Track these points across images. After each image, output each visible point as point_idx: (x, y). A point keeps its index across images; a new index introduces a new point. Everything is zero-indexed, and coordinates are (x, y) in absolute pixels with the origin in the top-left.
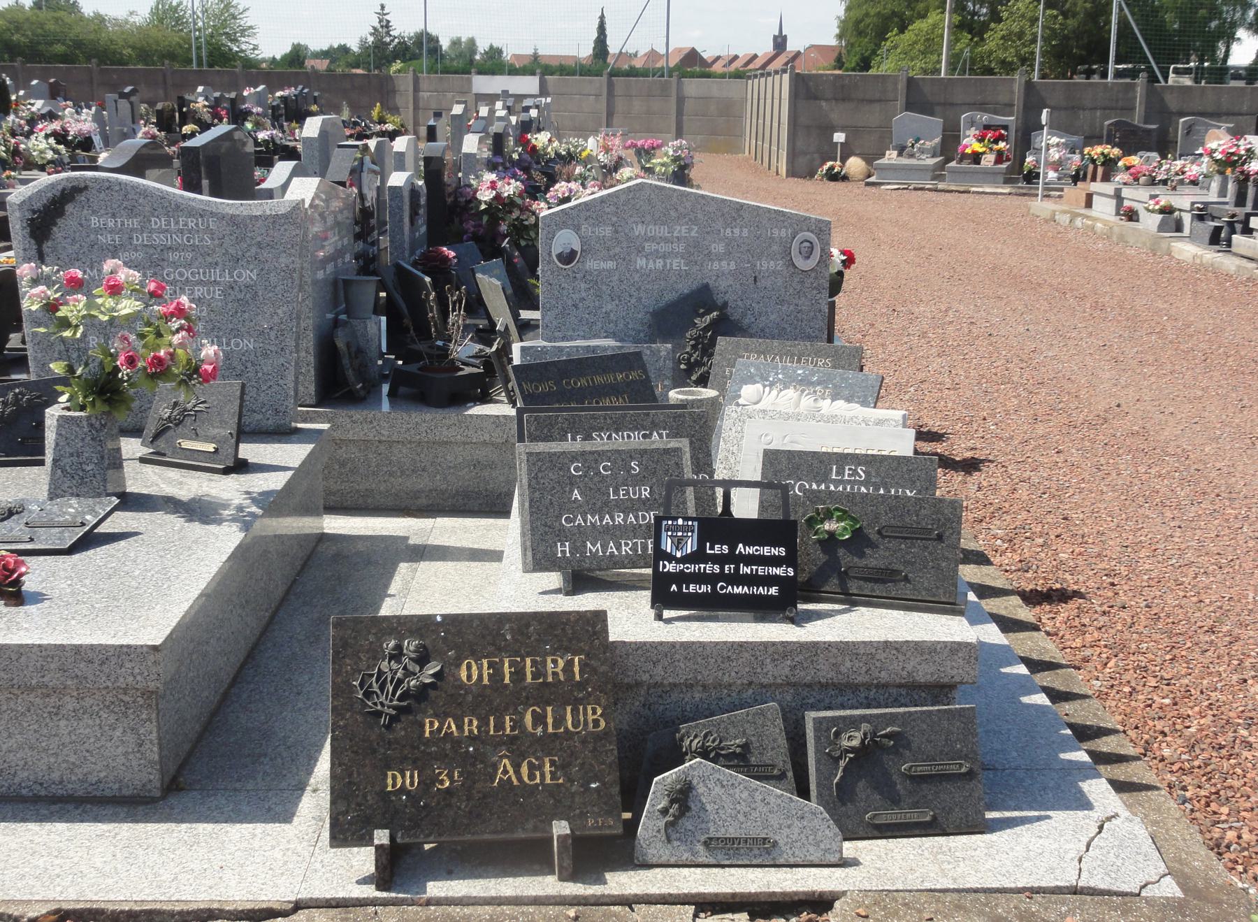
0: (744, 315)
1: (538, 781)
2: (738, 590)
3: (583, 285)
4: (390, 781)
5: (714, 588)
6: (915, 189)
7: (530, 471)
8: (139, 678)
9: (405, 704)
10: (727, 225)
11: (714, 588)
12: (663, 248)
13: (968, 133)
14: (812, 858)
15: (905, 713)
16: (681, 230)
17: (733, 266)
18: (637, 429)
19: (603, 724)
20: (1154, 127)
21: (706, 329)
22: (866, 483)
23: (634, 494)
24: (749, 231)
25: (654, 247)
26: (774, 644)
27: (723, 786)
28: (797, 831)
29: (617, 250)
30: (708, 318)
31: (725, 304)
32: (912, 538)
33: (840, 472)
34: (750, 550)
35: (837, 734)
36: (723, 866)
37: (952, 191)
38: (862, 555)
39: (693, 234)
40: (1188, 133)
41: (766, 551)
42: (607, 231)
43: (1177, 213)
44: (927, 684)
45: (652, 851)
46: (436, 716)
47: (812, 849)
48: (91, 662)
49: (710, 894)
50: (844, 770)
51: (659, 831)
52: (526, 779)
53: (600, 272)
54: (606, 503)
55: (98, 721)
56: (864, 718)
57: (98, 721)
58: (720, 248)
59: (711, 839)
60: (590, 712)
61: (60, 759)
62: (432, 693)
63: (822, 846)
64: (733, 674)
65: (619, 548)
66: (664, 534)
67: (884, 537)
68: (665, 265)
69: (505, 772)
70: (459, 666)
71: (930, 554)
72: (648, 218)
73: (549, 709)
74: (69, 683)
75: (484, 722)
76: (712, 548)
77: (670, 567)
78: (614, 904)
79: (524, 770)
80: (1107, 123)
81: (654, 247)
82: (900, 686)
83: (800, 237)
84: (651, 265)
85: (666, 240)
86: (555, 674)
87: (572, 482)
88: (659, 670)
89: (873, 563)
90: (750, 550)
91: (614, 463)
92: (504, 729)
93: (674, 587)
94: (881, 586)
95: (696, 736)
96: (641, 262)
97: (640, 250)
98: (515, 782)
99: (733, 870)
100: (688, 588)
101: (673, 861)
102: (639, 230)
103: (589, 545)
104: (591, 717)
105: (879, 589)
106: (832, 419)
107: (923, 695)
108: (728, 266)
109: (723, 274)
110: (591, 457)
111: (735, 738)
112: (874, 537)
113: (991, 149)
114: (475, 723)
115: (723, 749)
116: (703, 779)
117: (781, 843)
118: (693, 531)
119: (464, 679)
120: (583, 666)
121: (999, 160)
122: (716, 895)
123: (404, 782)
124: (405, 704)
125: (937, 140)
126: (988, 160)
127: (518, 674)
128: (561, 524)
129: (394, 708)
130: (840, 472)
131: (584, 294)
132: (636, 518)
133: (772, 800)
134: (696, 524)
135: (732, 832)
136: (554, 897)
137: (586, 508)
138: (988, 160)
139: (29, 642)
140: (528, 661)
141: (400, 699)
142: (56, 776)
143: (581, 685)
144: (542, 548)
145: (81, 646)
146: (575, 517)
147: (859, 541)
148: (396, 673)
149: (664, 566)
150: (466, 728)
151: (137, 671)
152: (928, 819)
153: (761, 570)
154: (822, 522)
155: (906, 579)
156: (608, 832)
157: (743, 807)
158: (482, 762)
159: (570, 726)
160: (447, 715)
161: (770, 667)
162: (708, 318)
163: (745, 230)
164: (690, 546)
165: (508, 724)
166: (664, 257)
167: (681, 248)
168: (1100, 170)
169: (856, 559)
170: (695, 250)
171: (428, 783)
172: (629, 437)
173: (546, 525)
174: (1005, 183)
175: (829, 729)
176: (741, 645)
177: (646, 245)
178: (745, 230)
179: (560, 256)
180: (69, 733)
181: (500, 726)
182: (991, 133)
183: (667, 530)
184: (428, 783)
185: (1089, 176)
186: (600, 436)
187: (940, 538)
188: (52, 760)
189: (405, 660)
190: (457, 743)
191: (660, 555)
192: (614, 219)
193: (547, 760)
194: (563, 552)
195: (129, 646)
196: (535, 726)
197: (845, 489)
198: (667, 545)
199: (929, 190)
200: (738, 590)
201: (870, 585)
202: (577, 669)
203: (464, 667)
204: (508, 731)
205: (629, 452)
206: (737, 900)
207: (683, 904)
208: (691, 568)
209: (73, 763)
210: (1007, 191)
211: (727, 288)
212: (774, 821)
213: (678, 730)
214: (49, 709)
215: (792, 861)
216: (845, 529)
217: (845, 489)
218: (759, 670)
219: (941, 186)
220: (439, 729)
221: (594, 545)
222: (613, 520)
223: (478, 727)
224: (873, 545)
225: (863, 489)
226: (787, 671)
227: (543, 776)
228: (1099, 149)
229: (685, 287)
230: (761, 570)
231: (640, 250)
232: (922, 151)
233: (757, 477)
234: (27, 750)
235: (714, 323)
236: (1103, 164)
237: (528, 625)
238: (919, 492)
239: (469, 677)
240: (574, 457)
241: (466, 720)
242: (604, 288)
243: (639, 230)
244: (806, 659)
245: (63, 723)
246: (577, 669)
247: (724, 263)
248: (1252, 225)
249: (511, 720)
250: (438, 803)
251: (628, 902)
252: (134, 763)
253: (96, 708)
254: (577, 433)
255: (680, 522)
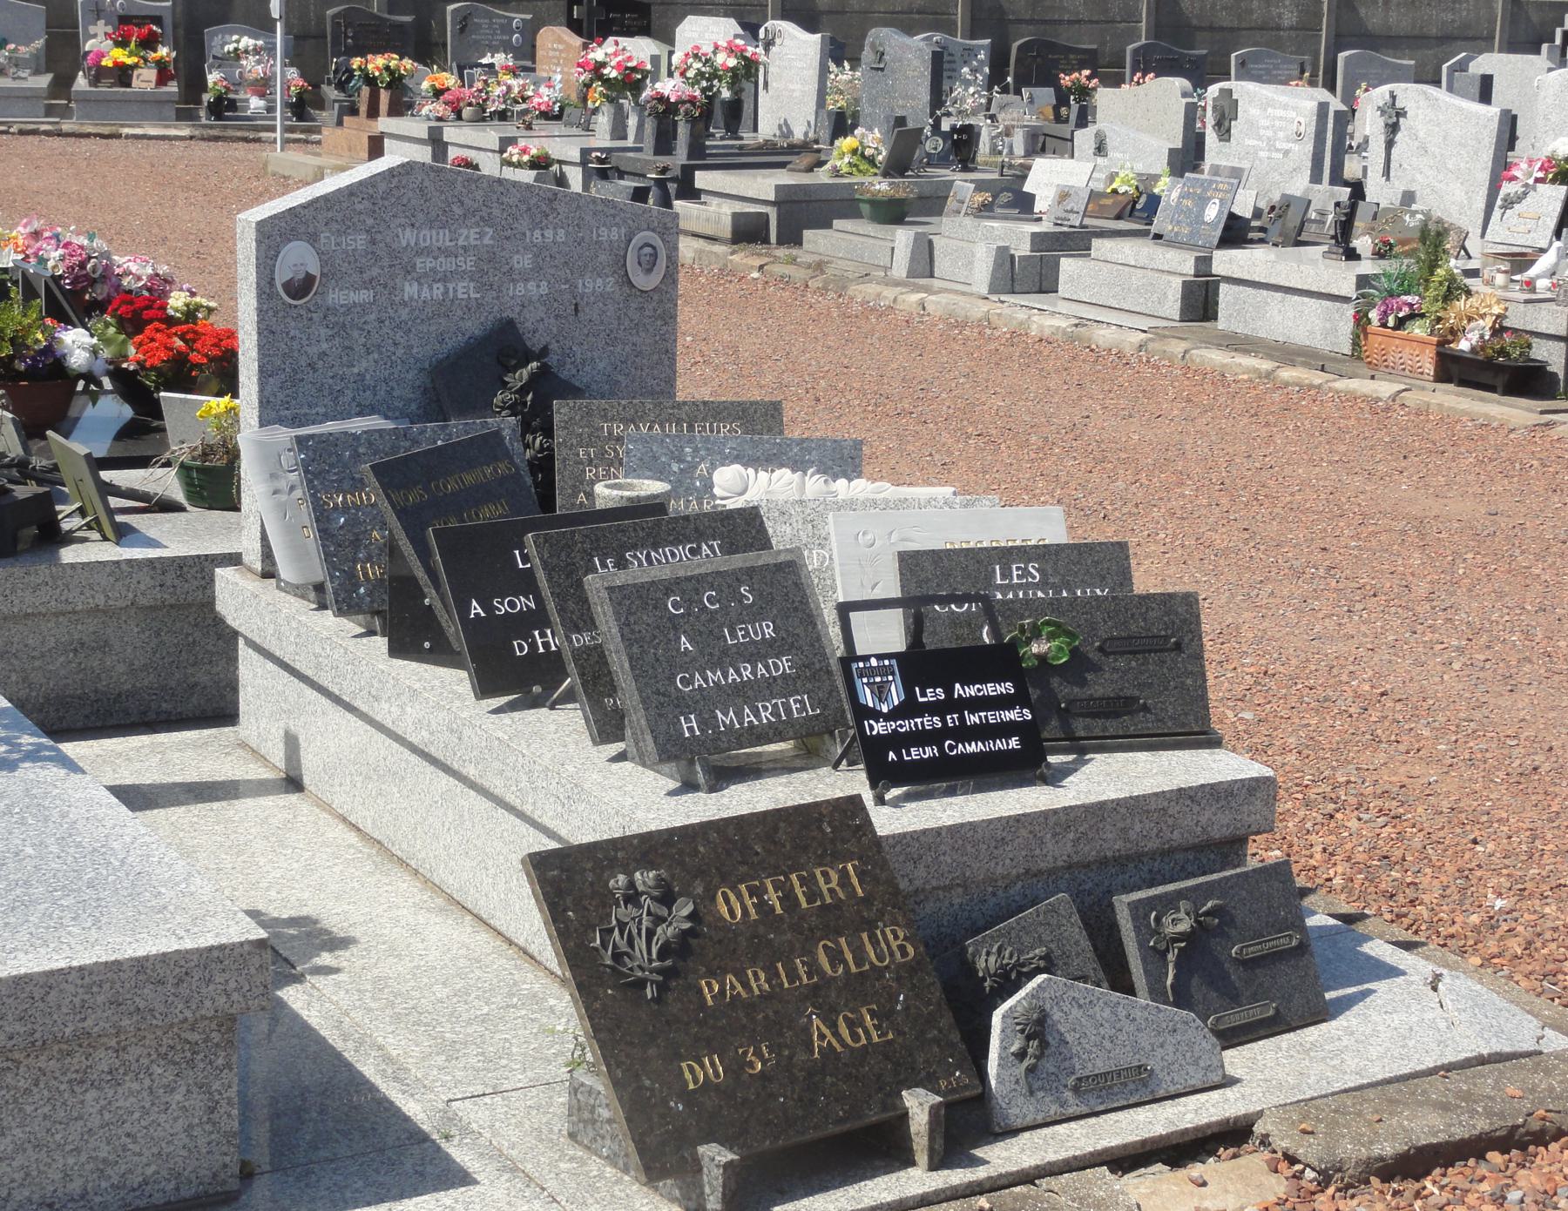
0: (562, 364)
1: (864, 1041)
2: (973, 748)
3: (323, 331)
4: (688, 1076)
5: (941, 749)
6: (22, 133)
7: (617, 614)
8: (235, 996)
9: (669, 963)
10: (535, 225)
11: (941, 749)
12: (445, 264)
13: (92, 30)
14: (1193, 1082)
15: (1221, 880)
16: (467, 235)
17: (544, 290)
18: (681, 542)
19: (910, 950)
20: (408, 19)
21: (523, 391)
22: (1043, 585)
23: (756, 633)
24: (567, 234)
25: (430, 263)
26: (1055, 811)
27: (1080, 1006)
28: (1171, 1049)
29: (375, 271)
30: (525, 373)
31: (545, 351)
32: (1144, 652)
33: (1006, 574)
34: (971, 691)
35: (1158, 919)
36: (1097, 1114)
37: (88, 135)
38: (1083, 683)
39: (487, 241)
40: (462, 30)
41: (990, 689)
42: (359, 241)
43: (555, 167)
44: (1205, 839)
45: (1014, 1111)
46: (711, 973)
47: (1191, 1069)
48: (161, 982)
49: (1117, 1147)
50: (1177, 965)
51: (1017, 1082)
52: (849, 1041)
53: (349, 309)
54: (726, 651)
55: (147, 1082)
56: (1180, 894)
57: (147, 1082)
58: (523, 261)
59: (1079, 1079)
60: (891, 937)
61: (83, 1158)
62: (693, 942)
63: (1202, 1064)
64: (1008, 861)
65: (757, 715)
66: (858, 683)
67: (1107, 654)
68: (446, 292)
69: (822, 1037)
70: (713, 899)
71: (1170, 669)
72: (421, 216)
73: (842, 940)
74: (125, 1022)
75: (772, 975)
76: (924, 694)
77: (879, 728)
78: (1015, 1185)
79: (844, 1031)
80: (330, 12)
81: (430, 263)
82: (1186, 850)
83: (637, 240)
84: (426, 294)
85: (446, 252)
86: (831, 891)
87: (675, 624)
88: (921, 872)
89: (1099, 691)
90: (971, 691)
91: (720, 591)
92: (800, 979)
93: (892, 756)
94: (1115, 723)
95: (988, 954)
96: (410, 290)
97: (409, 270)
98: (839, 1049)
99: (1113, 1116)
100: (909, 754)
101: (1040, 1119)
102: (408, 237)
103: (720, 715)
104: (894, 945)
105: (1112, 726)
106: (851, 505)
107: (1212, 856)
108: (536, 289)
109: (530, 301)
110: (690, 586)
111: (1032, 948)
112: (1094, 656)
113: (146, 60)
114: (762, 976)
115: (1023, 965)
116: (1057, 1001)
117: (1157, 1069)
118: (893, 674)
119: (727, 917)
120: (861, 875)
121: (163, 79)
122: (1125, 1146)
123: (706, 1075)
124: (669, 963)
125: (39, 43)
126: (145, 79)
127: (788, 899)
128: (676, 688)
129: (659, 971)
130: (1006, 574)
131: (325, 346)
132: (767, 667)
133: (1138, 1014)
134: (894, 662)
135: (1101, 1066)
136: (943, 1190)
137: (702, 661)
138: (145, 79)
139: (62, 964)
140: (794, 877)
141: (663, 954)
142: (75, 1186)
143: (867, 901)
144: (663, 728)
145: (147, 958)
146: (692, 676)
147: (1079, 665)
148: (640, 922)
149: (872, 728)
150: (754, 986)
151: (232, 985)
152: (1271, 1012)
153: (992, 717)
154: (1028, 642)
155: (1145, 708)
156: (967, 1094)
157: (1107, 1031)
158: (790, 1028)
159: (874, 959)
160: (725, 972)
161: (1050, 845)
162: (525, 373)
163: (561, 232)
164: (896, 696)
165: (802, 970)
166: (444, 280)
167: (468, 264)
168: (384, 97)
169: (1076, 690)
170: (491, 268)
171: (737, 1068)
172: (673, 555)
173: (658, 693)
174: (178, 119)
175: (1147, 916)
176: (1018, 819)
177: (418, 261)
178: (561, 232)
179: (287, 286)
180: (100, 1112)
181: (793, 975)
182: (134, 28)
183: (861, 677)
184: (737, 1068)
185: (363, 108)
186: (635, 556)
187: (1178, 647)
188: (71, 1161)
189: (647, 902)
190: (751, 1006)
191: (863, 713)
192: (370, 222)
193: (864, 1010)
194: (691, 729)
195: (222, 947)
196: (833, 967)
197: (1016, 595)
198: (867, 698)
199: (47, 133)
200: (973, 748)
201: (1100, 722)
202: (855, 881)
203: (720, 899)
204: (805, 980)
205: (734, 572)
206: (1148, 1148)
207: (947, 1200)
208: (906, 726)
209: (104, 1161)
210: (186, 132)
211: (537, 328)
212: (1144, 1041)
213: (965, 949)
214: (71, 1076)
215: (1173, 1090)
216: (1060, 649)
217: (1016, 595)
218: (1038, 852)
219: (67, 126)
220: (722, 991)
221: (726, 714)
222: (740, 675)
223: (768, 981)
224: (1097, 669)
225: (1040, 594)
226: (1069, 848)
227: (867, 1032)
228: (380, 61)
229: (473, 326)
230: (992, 717)
231: (409, 270)
232: (17, 63)
233: (895, 592)
234: (30, 1152)
235: (533, 377)
236: (389, 86)
237: (776, 829)
238: (1112, 590)
239: (732, 912)
240: (670, 587)
241: (749, 972)
242: (356, 334)
243: (408, 237)
244: (1091, 827)
245: (91, 1095)
246: (855, 881)
247: (531, 285)
248: (698, 185)
249: (803, 963)
250: (758, 1095)
251: (1028, 1177)
252: (202, 1142)
253: (145, 1061)
254: (606, 556)
255: (874, 662)
